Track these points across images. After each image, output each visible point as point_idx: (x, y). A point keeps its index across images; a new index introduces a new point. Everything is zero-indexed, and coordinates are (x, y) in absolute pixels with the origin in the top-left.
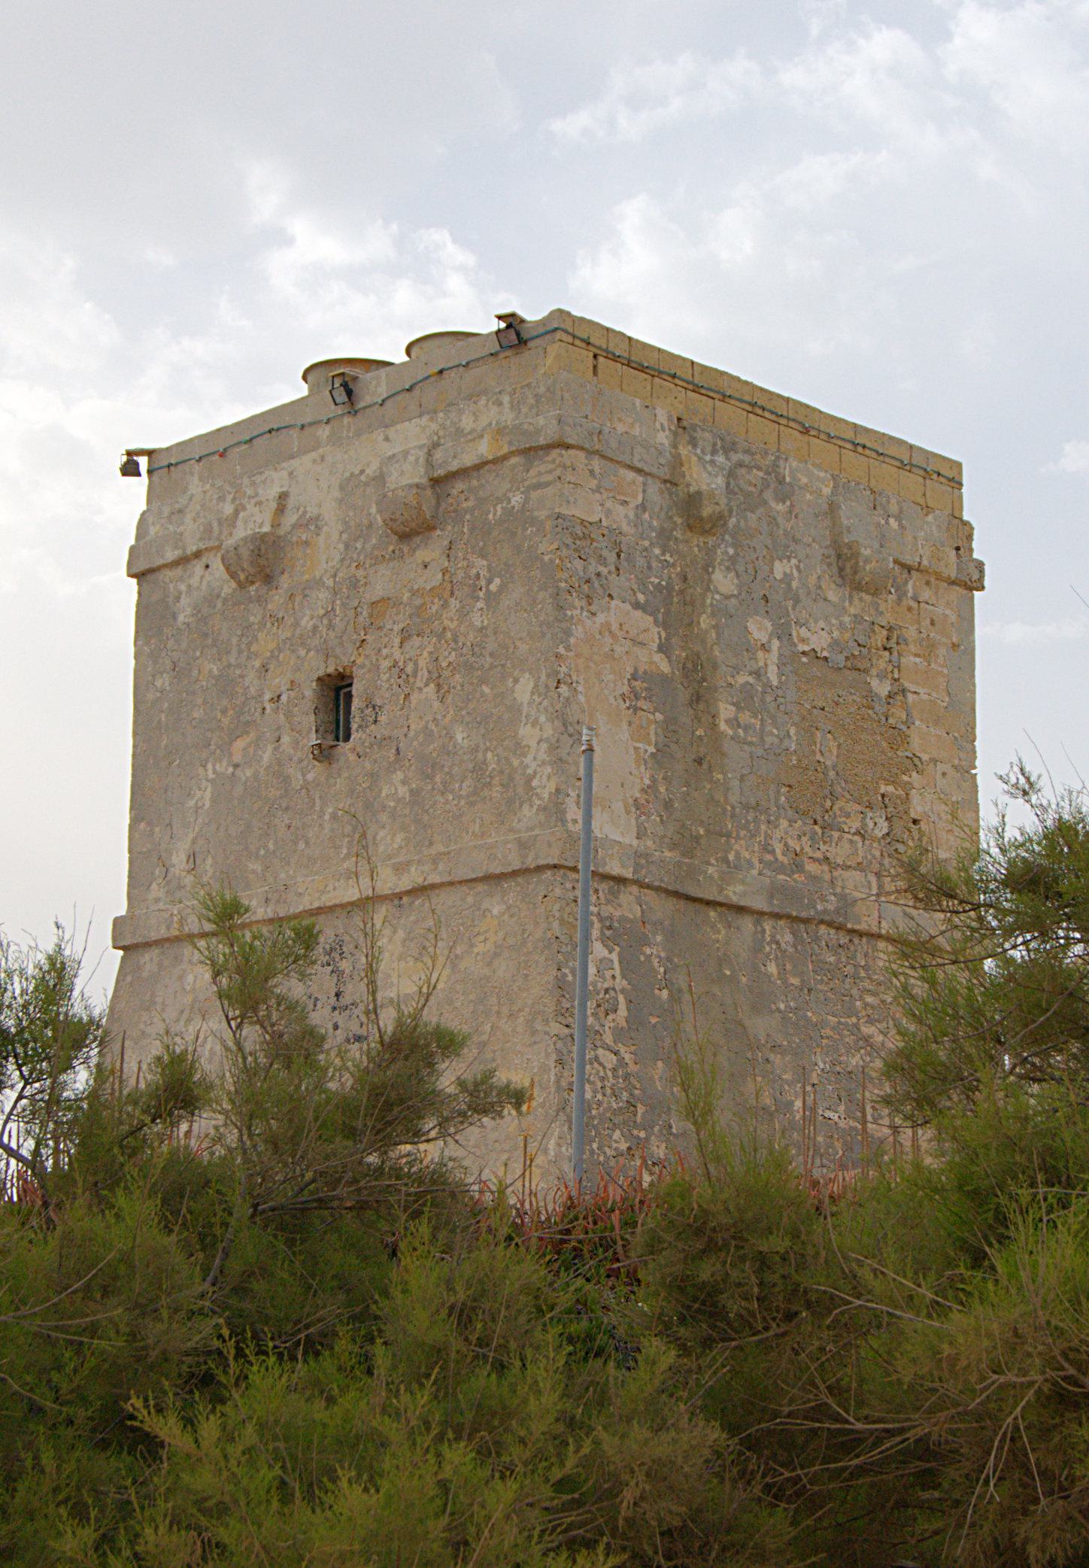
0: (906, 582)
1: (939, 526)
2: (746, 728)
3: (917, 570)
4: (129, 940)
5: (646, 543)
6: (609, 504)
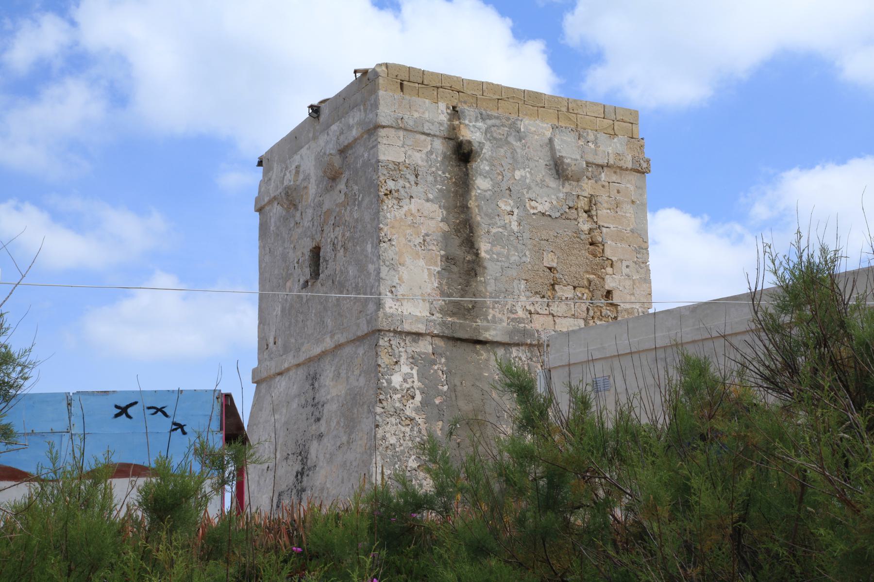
0: (600, 174)
1: (621, 144)
2: (498, 254)
3: (607, 166)
4: (259, 380)
5: (434, 169)
6: (409, 152)
